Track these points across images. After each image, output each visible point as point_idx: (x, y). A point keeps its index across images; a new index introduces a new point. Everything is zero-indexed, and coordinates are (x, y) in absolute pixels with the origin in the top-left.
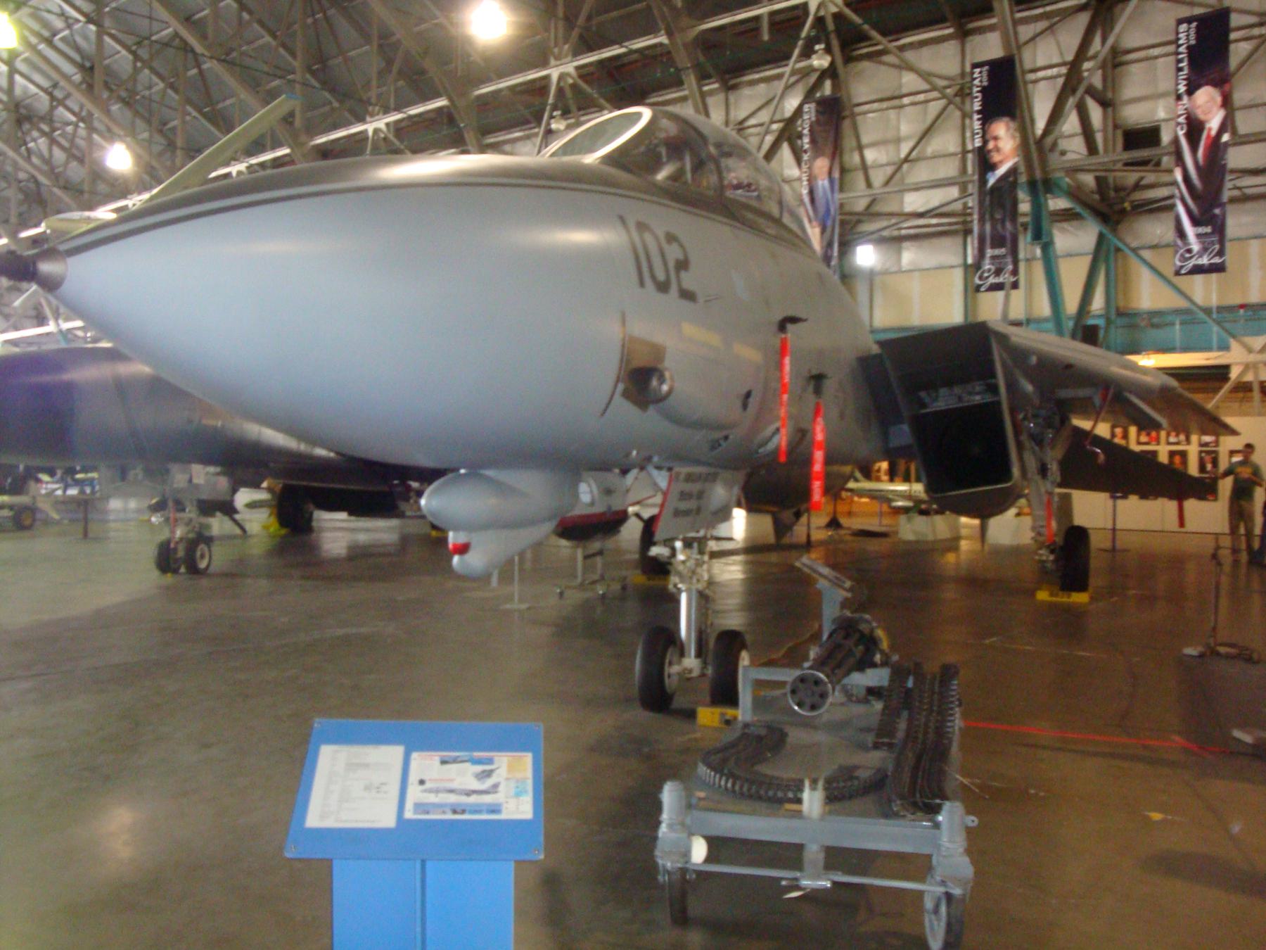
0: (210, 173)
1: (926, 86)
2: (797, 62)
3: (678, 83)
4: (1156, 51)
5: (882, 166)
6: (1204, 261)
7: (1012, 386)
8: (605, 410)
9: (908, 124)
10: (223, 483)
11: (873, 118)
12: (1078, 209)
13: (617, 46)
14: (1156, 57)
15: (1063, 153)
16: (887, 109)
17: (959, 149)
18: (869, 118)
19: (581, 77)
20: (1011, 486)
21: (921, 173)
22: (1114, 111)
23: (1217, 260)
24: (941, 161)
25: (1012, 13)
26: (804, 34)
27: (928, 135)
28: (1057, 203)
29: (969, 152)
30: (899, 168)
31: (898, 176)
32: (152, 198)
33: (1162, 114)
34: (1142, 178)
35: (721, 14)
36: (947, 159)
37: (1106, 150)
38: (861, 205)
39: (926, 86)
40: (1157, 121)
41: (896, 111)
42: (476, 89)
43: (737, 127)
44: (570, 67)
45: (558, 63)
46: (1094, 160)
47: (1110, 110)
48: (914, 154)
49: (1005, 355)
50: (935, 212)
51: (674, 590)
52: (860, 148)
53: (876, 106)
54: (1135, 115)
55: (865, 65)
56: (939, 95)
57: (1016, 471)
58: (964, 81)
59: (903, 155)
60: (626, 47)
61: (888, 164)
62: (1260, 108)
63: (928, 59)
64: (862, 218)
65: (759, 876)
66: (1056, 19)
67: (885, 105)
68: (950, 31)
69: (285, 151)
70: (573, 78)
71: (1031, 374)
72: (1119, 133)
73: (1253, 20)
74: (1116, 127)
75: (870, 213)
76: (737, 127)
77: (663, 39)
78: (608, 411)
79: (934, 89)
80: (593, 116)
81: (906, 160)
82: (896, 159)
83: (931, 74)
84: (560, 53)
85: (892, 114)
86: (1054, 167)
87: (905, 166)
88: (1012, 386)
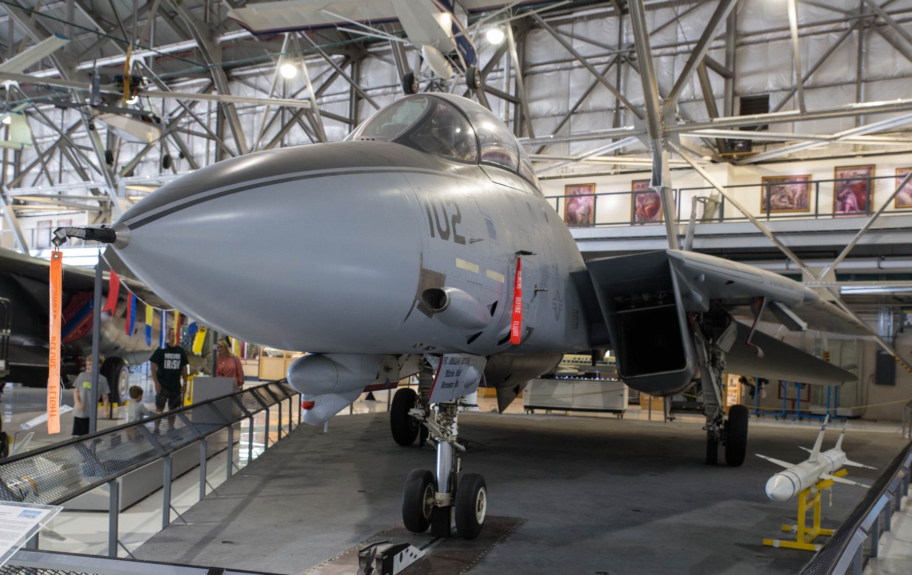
0: (79, 64)
4: (769, 36)
5: (554, 116)
7: (686, 296)
8: (406, 318)
14: (768, 41)
16: (560, 70)
17: (614, 106)
18: (546, 76)
20: (683, 372)
24: (600, 114)
27: (589, 95)
29: (622, 108)
30: (569, 117)
31: (567, 124)
32: (571, 13)
33: (771, 86)
36: (605, 113)
40: (767, 91)
41: (568, 71)
42: (221, 35)
43: (630, 49)
47: (731, 81)
49: (680, 273)
51: (431, 442)
53: (551, 66)
54: (749, 85)
56: (588, 61)
57: (689, 362)
59: (572, 106)
61: (559, 115)
62: (844, 87)
63: (592, 30)
65: (118, 257)
67: (559, 66)
68: (611, 9)
69: (192, 44)
71: (701, 287)
72: (737, 101)
73: (841, 16)
74: (735, 94)
76: (630, 49)
78: (408, 318)
81: (573, 112)
82: (565, 111)
85: (564, 74)
88: (686, 296)
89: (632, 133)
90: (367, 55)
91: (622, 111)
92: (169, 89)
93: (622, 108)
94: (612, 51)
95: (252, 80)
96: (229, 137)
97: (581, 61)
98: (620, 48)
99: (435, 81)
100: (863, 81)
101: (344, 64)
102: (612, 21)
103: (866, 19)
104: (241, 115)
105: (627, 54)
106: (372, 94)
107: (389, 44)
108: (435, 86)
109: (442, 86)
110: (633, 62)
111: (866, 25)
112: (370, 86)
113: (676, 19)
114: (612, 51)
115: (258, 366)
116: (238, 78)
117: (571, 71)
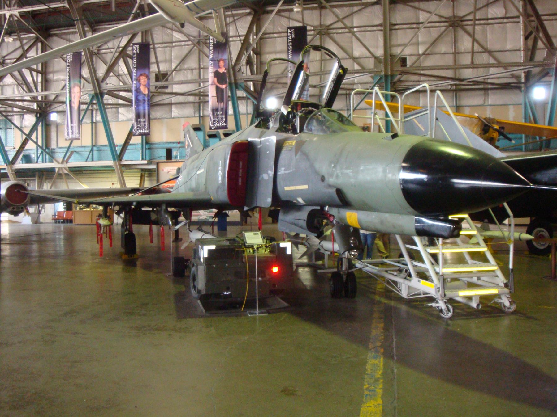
1: (186, 39)
2: (281, 6)
3: (72, 25)
6: (220, 125)
9: (177, 53)
10: (402, 284)
11: (160, 50)
12: (249, 96)
13: (43, 5)
15: (106, 84)
17: (198, 67)
19: (21, 16)
21: (178, 77)
22: (260, 57)
23: (224, 124)
25: (224, 12)
26: (134, 11)
28: (240, 93)
29: (201, 68)
34: (273, 86)
35: (40, 4)
37: (257, 74)
38: (52, 97)
39: (186, 39)
43: (98, 49)
44: (16, 12)
45: (9, 9)
46: (253, 77)
47: (259, 56)
48: (178, 68)
50: (189, 93)
52: (157, 63)
55: (55, 38)
58: (322, 28)
59: (173, 67)
60: (48, 6)
64: (155, 94)
66: (363, 7)
70: (17, 17)
75: (55, 101)
76: (98, 49)
77: (67, 5)
79: (189, 40)
80: (115, 25)
81: (175, 70)
83: (190, 36)
84: (10, 4)
86: (103, 88)
87: (174, 72)
89: (452, 67)
90: (50, 36)
91: (202, 70)
92: (328, 7)
93: (201, 68)
94: (195, 39)
95: (64, 36)
96: (154, 63)
97: (192, 42)
98: (199, 37)
99: (94, 51)
100: (323, 60)
101: (37, 40)
102: (317, 12)
103: (201, 40)
104: (231, 41)
105: (96, 51)
106: (105, 52)
107: (76, 28)
108: (94, 54)
109: (98, 54)
110: (207, 45)
111: (323, 33)
112: (398, 22)
113: (351, 14)
114: (195, 39)
115: (90, 223)
116: (56, 35)
117: (173, 48)
